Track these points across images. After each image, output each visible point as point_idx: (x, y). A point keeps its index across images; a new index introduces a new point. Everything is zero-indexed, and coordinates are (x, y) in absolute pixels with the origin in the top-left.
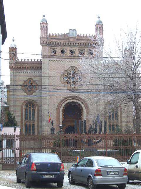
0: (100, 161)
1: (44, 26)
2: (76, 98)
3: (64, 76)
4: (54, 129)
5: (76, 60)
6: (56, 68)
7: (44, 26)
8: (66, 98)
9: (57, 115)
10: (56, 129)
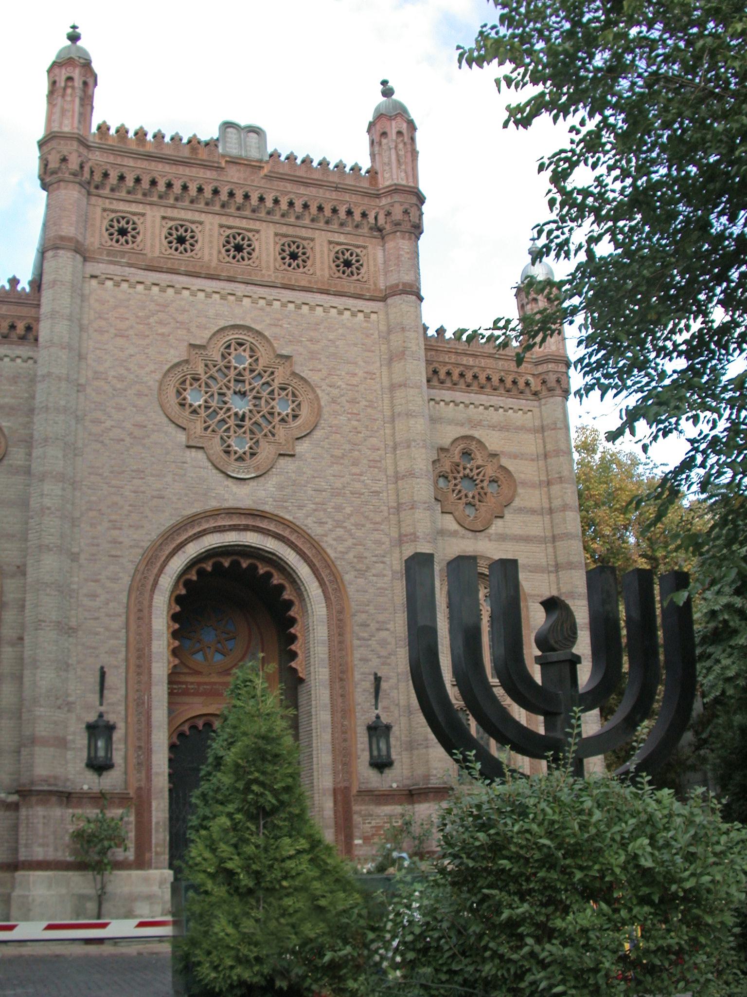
0: (279, 281)
1: (73, 76)
2: (264, 525)
3: (182, 377)
4: (110, 728)
5: (262, 291)
6: (132, 327)
7: (73, 76)
8: (193, 520)
9: (133, 627)
10: (121, 725)
